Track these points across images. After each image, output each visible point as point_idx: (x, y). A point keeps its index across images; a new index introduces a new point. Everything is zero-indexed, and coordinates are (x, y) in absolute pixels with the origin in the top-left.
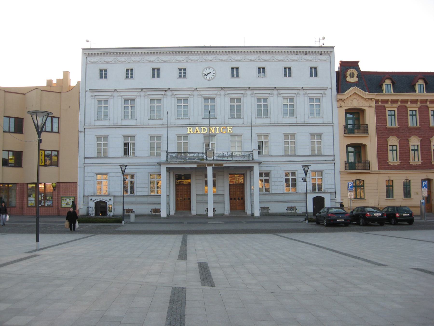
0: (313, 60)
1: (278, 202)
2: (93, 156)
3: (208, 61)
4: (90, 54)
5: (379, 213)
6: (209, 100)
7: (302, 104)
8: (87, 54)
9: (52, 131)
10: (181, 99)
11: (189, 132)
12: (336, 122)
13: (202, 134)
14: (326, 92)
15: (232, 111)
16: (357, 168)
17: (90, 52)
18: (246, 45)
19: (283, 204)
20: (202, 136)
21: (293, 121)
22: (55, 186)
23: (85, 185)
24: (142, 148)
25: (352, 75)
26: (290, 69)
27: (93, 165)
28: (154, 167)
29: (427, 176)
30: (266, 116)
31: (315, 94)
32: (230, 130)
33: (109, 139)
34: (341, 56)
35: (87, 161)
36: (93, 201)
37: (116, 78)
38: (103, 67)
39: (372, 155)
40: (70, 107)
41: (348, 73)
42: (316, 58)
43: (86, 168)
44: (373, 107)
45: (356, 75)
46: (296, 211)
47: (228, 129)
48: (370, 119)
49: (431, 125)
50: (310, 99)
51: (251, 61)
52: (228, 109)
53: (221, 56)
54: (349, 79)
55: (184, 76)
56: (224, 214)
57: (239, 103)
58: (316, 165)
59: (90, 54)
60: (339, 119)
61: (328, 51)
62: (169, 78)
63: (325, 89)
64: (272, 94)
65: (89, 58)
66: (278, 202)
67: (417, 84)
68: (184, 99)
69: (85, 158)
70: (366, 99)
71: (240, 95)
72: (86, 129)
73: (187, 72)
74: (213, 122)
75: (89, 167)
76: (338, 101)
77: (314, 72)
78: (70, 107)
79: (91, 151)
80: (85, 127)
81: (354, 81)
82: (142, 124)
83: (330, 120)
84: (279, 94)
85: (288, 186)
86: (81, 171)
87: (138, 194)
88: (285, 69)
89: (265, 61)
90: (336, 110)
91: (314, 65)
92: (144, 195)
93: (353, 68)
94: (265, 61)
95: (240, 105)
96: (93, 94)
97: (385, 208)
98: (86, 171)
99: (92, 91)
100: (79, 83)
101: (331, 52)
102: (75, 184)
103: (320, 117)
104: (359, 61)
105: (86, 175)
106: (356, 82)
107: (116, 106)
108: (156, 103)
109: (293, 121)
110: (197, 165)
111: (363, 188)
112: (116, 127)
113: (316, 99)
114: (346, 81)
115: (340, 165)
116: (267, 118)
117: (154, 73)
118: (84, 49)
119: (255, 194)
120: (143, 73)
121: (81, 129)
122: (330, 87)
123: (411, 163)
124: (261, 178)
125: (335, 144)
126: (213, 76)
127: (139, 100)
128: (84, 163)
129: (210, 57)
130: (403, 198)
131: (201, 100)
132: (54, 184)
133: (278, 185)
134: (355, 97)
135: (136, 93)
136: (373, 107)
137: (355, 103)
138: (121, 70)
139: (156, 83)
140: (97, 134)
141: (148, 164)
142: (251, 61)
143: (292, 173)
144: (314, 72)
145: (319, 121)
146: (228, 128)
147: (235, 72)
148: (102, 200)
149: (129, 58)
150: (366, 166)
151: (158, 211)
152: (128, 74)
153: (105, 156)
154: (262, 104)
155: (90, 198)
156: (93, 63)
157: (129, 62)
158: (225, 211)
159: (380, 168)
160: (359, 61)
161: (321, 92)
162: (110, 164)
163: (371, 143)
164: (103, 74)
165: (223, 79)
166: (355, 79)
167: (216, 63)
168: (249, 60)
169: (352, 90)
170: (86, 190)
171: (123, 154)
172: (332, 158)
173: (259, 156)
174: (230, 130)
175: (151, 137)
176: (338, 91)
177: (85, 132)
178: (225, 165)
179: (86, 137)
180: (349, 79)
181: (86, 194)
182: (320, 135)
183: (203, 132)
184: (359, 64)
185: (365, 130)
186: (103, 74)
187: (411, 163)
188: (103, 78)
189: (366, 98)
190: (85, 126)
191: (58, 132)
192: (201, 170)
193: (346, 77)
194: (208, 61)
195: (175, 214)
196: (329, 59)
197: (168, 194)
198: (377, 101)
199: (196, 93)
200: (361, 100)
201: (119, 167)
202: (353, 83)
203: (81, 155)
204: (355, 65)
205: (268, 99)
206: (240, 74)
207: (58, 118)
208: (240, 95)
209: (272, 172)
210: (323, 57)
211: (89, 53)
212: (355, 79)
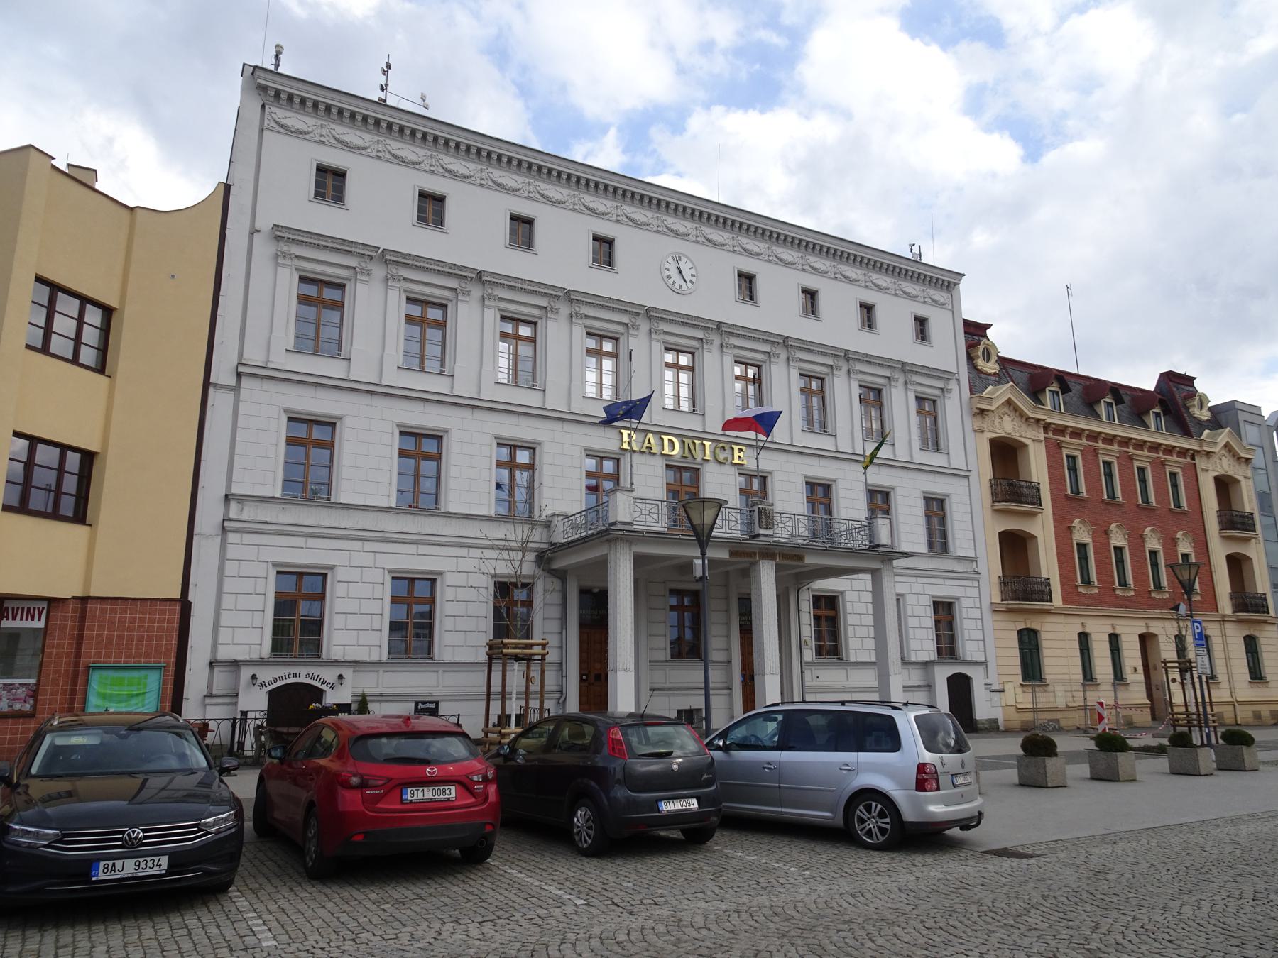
2: (383, 503)
3: (749, 253)
5: (282, 733)
8: (272, 93)
13: (733, 470)
20: (660, 464)
24: (470, 479)
30: (824, 428)
34: (972, 309)
36: (262, 685)
39: (1048, 564)
43: (232, 537)
53: (634, 209)
58: (941, 581)
61: (945, 282)
70: (1028, 419)
71: (824, 370)
72: (244, 380)
75: (248, 538)
80: (241, 369)
84: (578, 315)
98: (232, 552)
99: (281, 234)
103: (442, 373)
104: (989, 326)
111: (426, 632)
126: (669, 277)
127: (362, 289)
137: (1008, 427)
148: (302, 680)
153: (435, 509)
155: (246, 673)
160: (989, 326)
163: (1043, 529)
167: (698, 246)
170: (224, 635)
174: (742, 454)
175: (290, 419)
181: (225, 653)
183: (666, 451)
194: (749, 253)
200: (1017, 422)
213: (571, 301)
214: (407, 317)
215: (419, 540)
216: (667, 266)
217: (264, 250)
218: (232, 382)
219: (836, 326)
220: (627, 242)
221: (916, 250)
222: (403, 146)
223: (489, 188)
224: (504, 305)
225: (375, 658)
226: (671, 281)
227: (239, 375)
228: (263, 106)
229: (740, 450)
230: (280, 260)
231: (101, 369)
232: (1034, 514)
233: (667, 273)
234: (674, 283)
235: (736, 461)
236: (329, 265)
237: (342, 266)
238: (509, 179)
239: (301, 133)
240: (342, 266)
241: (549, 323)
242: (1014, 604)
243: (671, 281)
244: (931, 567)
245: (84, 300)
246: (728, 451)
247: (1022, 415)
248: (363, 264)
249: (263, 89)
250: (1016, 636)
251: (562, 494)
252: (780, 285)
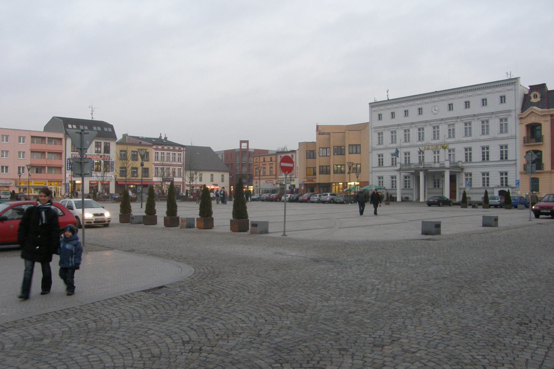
0: (502, 91)
1: (476, 194)
3: (434, 102)
6: (436, 128)
14: (511, 113)
25: (535, 96)
34: (526, 83)
61: (513, 82)
63: (509, 111)
66: (476, 194)
83: (514, 133)
93: (537, 91)
99: (375, 128)
118: (370, 104)
121: (370, 151)
122: (513, 109)
125: (517, 152)
129: (435, 99)
135: (489, 116)
137: (533, 120)
138: (479, 100)
156: (374, 111)
164: (380, 117)
171: (481, 159)
172: (514, 162)
186: (380, 117)
191: (360, 153)
194: (434, 102)
203: (371, 166)
206: (506, 100)
210: (510, 87)
211: (373, 105)
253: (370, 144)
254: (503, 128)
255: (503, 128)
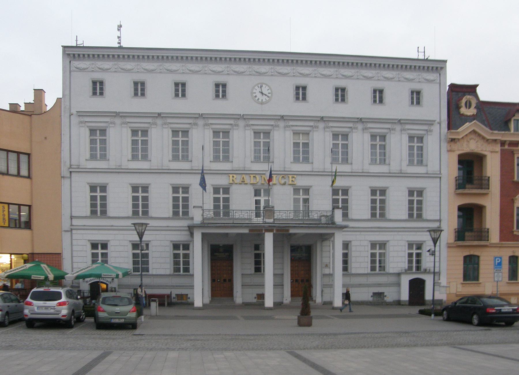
1: (360, 285)
2: (84, 215)
3: (260, 74)
4: (341, 64)
7: (398, 145)
8: (72, 56)
9: (18, 175)
10: (260, 133)
11: (231, 182)
12: (444, 172)
14: (432, 128)
15: (175, 150)
16: (466, 238)
17: (76, 52)
18: (292, 51)
19: (367, 288)
21: (383, 169)
22: (26, 258)
23: (74, 258)
24: (161, 203)
25: (468, 105)
26: (343, 90)
27: (84, 228)
28: (179, 233)
29: (513, 252)
31: (417, 130)
32: (294, 179)
33: (109, 189)
34: (455, 76)
35: (75, 222)
37: (118, 95)
38: (98, 76)
39: (492, 221)
40: (46, 138)
41: (464, 101)
42: (316, 72)
43: (74, 232)
44: (497, 152)
45: (474, 105)
46: (189, 300)
47: (291, 179)
48: (493, 168)
49: (516, 179)
50: (214, 132)
51: (325, 76)
52: (290, 149)
53: (280, 67)
54: (464, 110)
55: (224, 96)
56: (282, 303)
57: (344, 140)
59: (341, 64)
60: (451, 170)
61: (438, 67)
62: (200, 97)
63: (430, 123)
64: (355, 128)
65: (74, 62)
67: (513, 119)
68: (223, 132)
69: (72, 217)
70: (488, 140)
71: (385, 131)
72: (73, 174)
73: (229, 90)
74: (342, 168)
75: (79, 232)
76: (448, 142)
77: (416, 97)
78: (46, 138)
79: (83, 207)
80: (71, 170)
81: (472, 114)
82: (160, 168)
85: (94, 262)
86: (66, 237)
87: (154, 273)
88: (297, 88)
89: (346, 77)
90: (445, 156)
91: (416, 86)
92: (163, 273)
94: (346, 77)
95: (228, 142)
96: (287, 124)
97: (465, 297)
98: (74, 237)
99: (81, 114)
100: (59, 100)
101: (442, 68)
102: (59, 255)
104: (477, 86)
105: (74, 242)
106: (473, 115)
107: (119, 140)
108: (262, 137)
109: (383, 169)
110: (250, 231)
112: (119, 171)
113: (264, 133)
114: (459, 113)
115: (448, 236)
116: (188, 161)
117: (177, 90)
118: (64, 47)
119: (195, 275)
120: (160, 87)
122: (438, 120)
123: (515, 233)
124: (411, 251)
126: (256, 96)
128: (72, 225)
129: (264, 68)
130: (462, 282)
131: (249, 134)
132: (25, 256)
133: (361, 263)
134: (472, 136)
136: (497, 152)
137: (473, 146)
139: (180, 106)
140: (131, 182)
141: (168, 229)
142: (325, 76)
143: (102, 244)
144: (416, 97)
145: (420, 170)
146: (290, 176)
147: (301, 93)
149: (115, 65)
150: (482, 235)
151: (261, 297)
152: (136, 90)
154: (262, 140)
157: (180, 71)
158: (284, 299)
159: (502, 239)
160: (477, 86)
161: (425, 127)
162: (112, 228)
163: (492, 205)
165: (285, 104)
166: (472, 111)
168: (190, 71)
169: (467, 127)
173: (343, 220)
174: (294, 179)
176: (449, 127)
177: (70, 177)
178: (292, 231)
179: (73, 185)
180: (464, 110)
182: (420, 193)
184: (478, 90)
185: (484, 184)
186: (98, 88)
187: (515, 233)
188: (180, 96)
189: (488, 138)
190: (70, 167)
192: (254, 239)
193: (458, 107)
194: (260, 74)
195: (211, 302)
196: (439, 79)
197: (279, 272)
198: (503, 143)
199: (201, 122)
200: (481, 142)
201: (428, 233)
202: (470, 116)
203: (66, 213)
204: (471, 89)
205: (231, 134)
207: (29, 155)
208: (385, 131)
209: (353, 243)
212: (472, 111)
213: (245, 119)
214: (294, 143)
215: (380, 230)
216: (254, 91)
217: (75, 120)
218: (69, 175)
219: (359, 104)
220: (234, 85)
221: (421, 50)
222: (81, 62)
223: (361, 79)
224: (214, 126)
225: (366, 272)
226: (257, 98)
227: (71, 172)
228: (70, 62)
229: (293, 177)
230: (164, 126)
231: (29, 177)
232: (486, 194)
233: (254, 95)
234: (258, 99)
235: (290, 183)
236: (98, 123)
237: (307, 126)
238: (409, 75)
239: (85, 69)
240: (307, 126)
241: (234, 131)
242: (460, 243)
243: (257, 98)
244: (370, 226)
245: (18, 153)
246: (287, 178)
247: (483, 138)
248: (316, 124)
249: (69, 55)
250: (462, 259)
251: (202, 205)
252: (282, 88)
253: (65, 154)
254: (417, 155)
255: (417, 155)
